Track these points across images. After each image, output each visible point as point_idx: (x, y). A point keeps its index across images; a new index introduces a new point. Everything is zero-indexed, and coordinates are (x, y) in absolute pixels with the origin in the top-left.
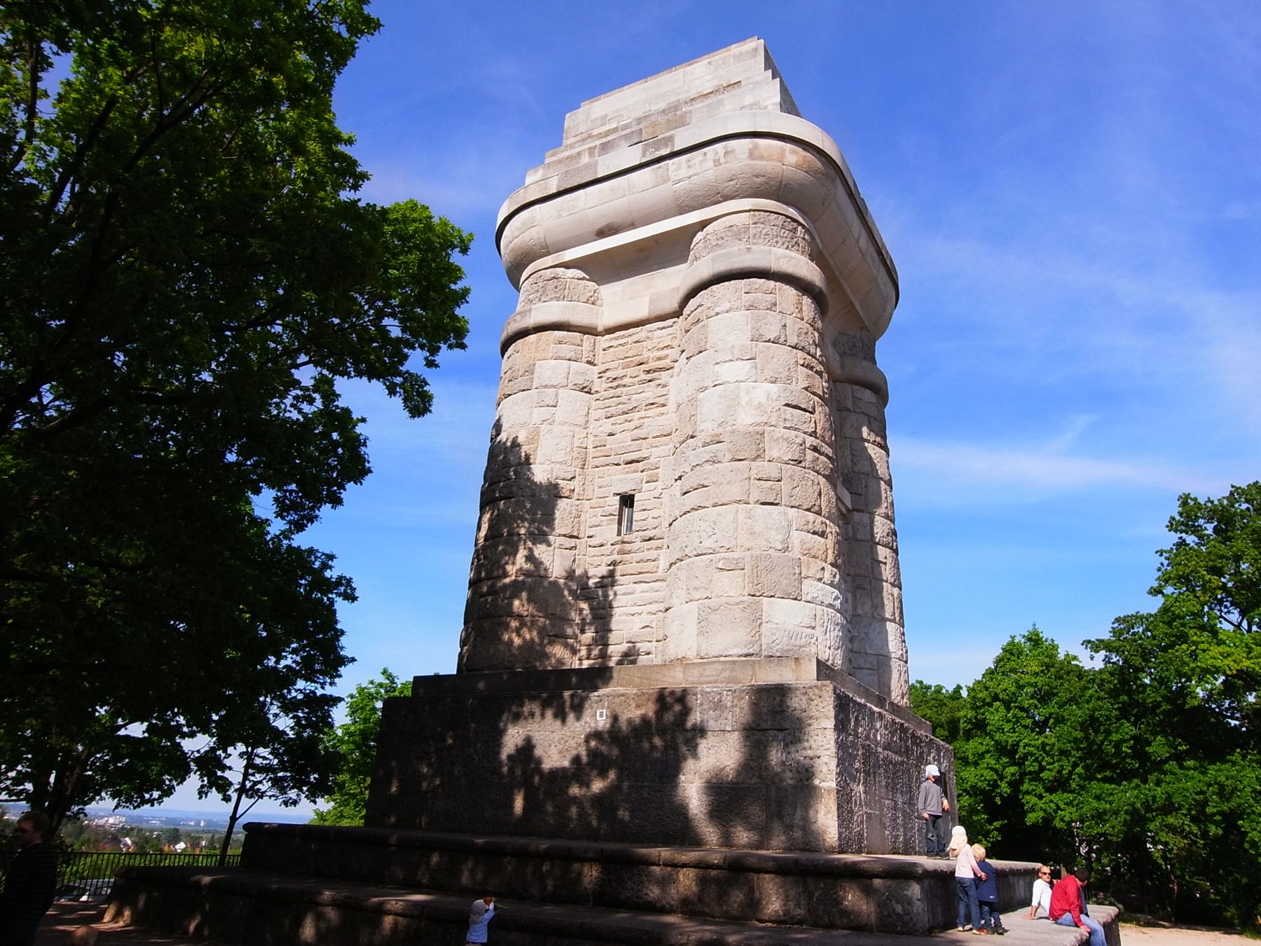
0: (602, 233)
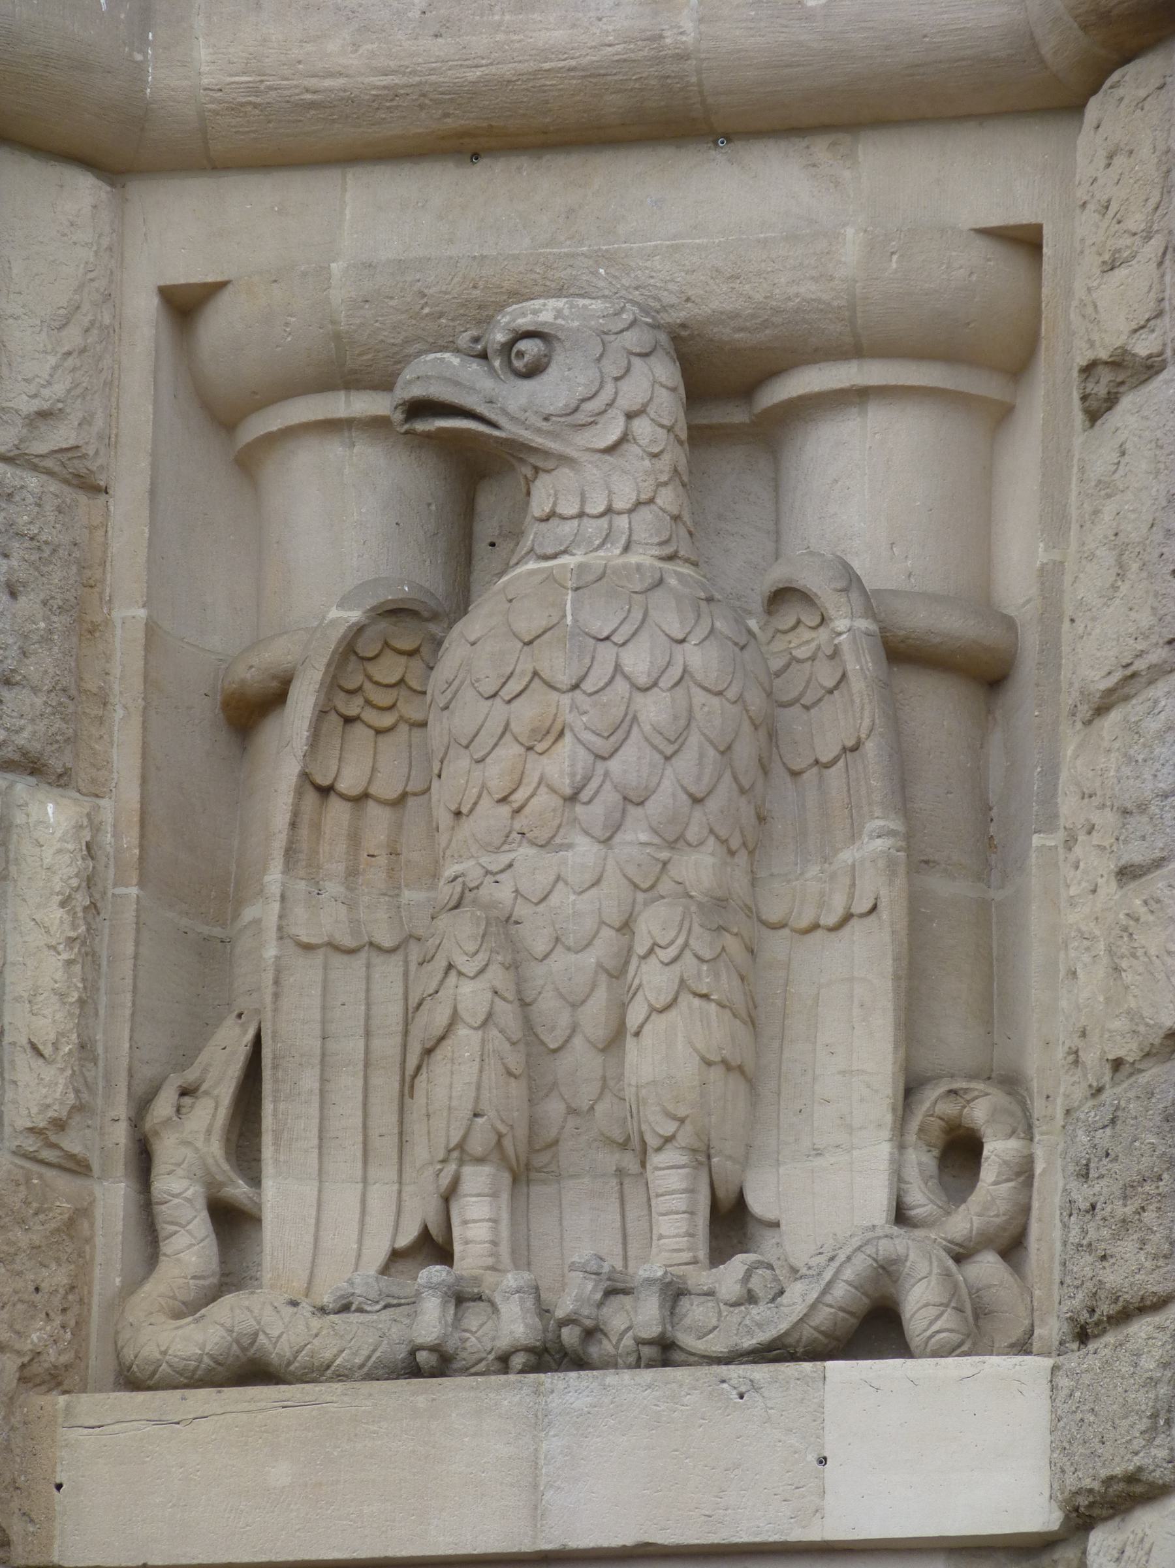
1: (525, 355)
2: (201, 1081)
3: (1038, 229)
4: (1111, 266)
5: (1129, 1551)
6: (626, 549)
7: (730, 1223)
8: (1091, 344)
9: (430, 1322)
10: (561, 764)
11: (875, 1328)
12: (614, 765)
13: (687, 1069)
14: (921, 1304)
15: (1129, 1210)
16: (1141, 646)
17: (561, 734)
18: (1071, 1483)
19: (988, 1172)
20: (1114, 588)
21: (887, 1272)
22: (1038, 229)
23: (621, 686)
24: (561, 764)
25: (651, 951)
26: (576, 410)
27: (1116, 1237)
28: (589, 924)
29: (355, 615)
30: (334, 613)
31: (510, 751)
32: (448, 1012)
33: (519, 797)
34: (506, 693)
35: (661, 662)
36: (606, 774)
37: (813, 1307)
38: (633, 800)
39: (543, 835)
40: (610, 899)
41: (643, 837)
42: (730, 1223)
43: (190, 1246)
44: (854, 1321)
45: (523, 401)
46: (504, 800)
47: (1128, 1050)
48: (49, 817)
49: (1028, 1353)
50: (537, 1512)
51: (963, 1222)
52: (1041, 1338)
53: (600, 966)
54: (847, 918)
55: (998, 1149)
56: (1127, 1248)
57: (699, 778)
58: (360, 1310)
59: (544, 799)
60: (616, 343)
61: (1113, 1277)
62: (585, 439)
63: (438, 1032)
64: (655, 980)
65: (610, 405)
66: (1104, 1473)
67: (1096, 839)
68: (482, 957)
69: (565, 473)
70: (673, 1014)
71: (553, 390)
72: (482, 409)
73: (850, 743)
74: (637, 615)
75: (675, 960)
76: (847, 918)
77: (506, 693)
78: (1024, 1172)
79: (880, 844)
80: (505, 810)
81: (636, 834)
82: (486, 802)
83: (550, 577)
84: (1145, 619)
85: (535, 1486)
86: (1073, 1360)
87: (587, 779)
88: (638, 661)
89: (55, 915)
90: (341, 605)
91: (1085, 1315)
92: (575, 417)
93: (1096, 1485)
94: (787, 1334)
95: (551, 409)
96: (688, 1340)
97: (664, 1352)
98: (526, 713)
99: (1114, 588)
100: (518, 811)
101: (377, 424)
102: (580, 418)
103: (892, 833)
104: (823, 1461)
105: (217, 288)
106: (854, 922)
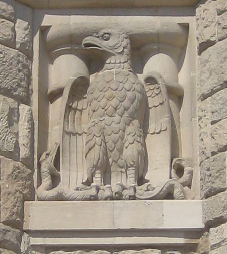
1: (106, 37)
2: (50, 153)
3: (188, 24)
4: (205, 27)
5: (219, 231)
6: (123, 69)
7: (141, 181)
8: (202, 39)
9: (93, 192)
11: (168, 195)
12: (123, 103)
13: (136, 153)
14: (176, 192)
15: (218, 174)
16: (215, 85)
17: (114, 97)
18: (207, 219)
19: (185, 173)
20: (209, 77)
21: (172, 187)
22: (188, 24)
23: (124, 90)
24: (114, 102)
25: (129, 134)
26: (115, 46)
27: (215, 179)
28: (118, 129)
29: (75, 78)
30: (72, 78)
31: (104, 100)
32: (94, 143)
33: (106, 108)
34: (104, 90)
35: (131, 87)
36: (121, 105)
37: (160, 192)
38: (126, 109)
39: (110, 114)
40: (121, 125)
41: (128, 115)
42: (141, 181)
43: (47, 181)
44: (51, 180)
45: (106, 44)
46: (103, 109)
47: (216, 150)
48: (24, 109)
49: (173, 198)
50: (114, 223)
51: (182, 180)
52: (9, 162)
53: (120, 137)
54: (161, 131)
55: (187, 169)
56: (217, 181)
57: (137, 106)
58: (80, 190)
59: (111, 108)
60: (121, 36)
61: (214, 186)
62: (116, 51)
63: (92, 145)
64: (130, 139)
65: (121, 45)
66: (214, 217)
67: (206, 117)
68: (100, 134)
69: (113, 57)
70: (133, 144)
71: (111, 42)
72: (98, 45)
73: (161, 102)
74: (126, 79)
75: (133, 136)
76: (161, 131)
77: (104, 90)
78: (191, 173)
79: (167, 119)
80: (103, 110)
81: (126, 114)
82: (100, 108)
83: (110, 73)
84: (216, 81)
85: (113, 219)
86: (205, 200)
87: (118, 105)
88: (127, 86)
89: (26, 124)
90: (73, 76)
91: (208, 193)
92: (114, 47)
93: (212, 219)
94: (156, 195)
95: (110, 45)
96: (137, 196)
97: (133, 198)
98: (107, 94)
99: (209, 77)
100: (106, 110)
102: (115, 47)
103: (169, 117)
104: (163, 216)
105: (50, 26)
106: (162, 132)
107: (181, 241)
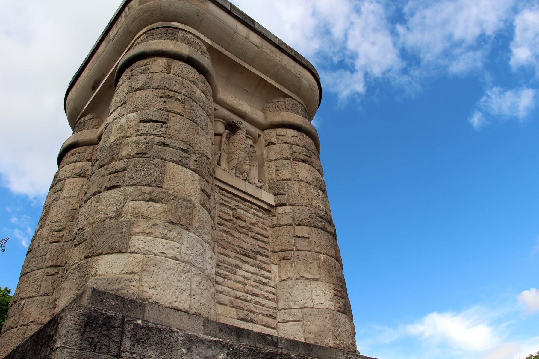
0: (94, 88)
10: (243, 146)
24: (243, 146)
101: (224, 123)
107: (266, 207)
